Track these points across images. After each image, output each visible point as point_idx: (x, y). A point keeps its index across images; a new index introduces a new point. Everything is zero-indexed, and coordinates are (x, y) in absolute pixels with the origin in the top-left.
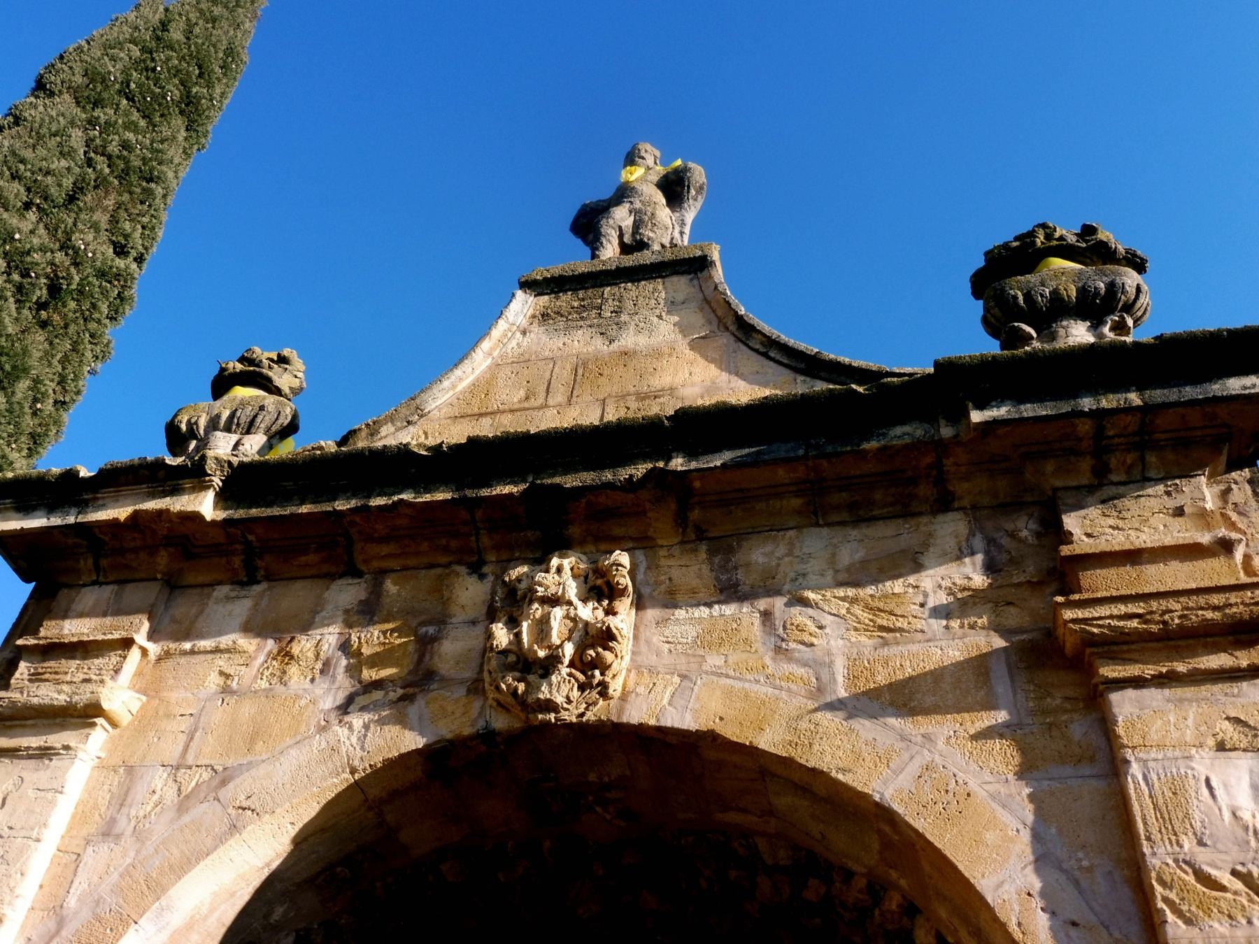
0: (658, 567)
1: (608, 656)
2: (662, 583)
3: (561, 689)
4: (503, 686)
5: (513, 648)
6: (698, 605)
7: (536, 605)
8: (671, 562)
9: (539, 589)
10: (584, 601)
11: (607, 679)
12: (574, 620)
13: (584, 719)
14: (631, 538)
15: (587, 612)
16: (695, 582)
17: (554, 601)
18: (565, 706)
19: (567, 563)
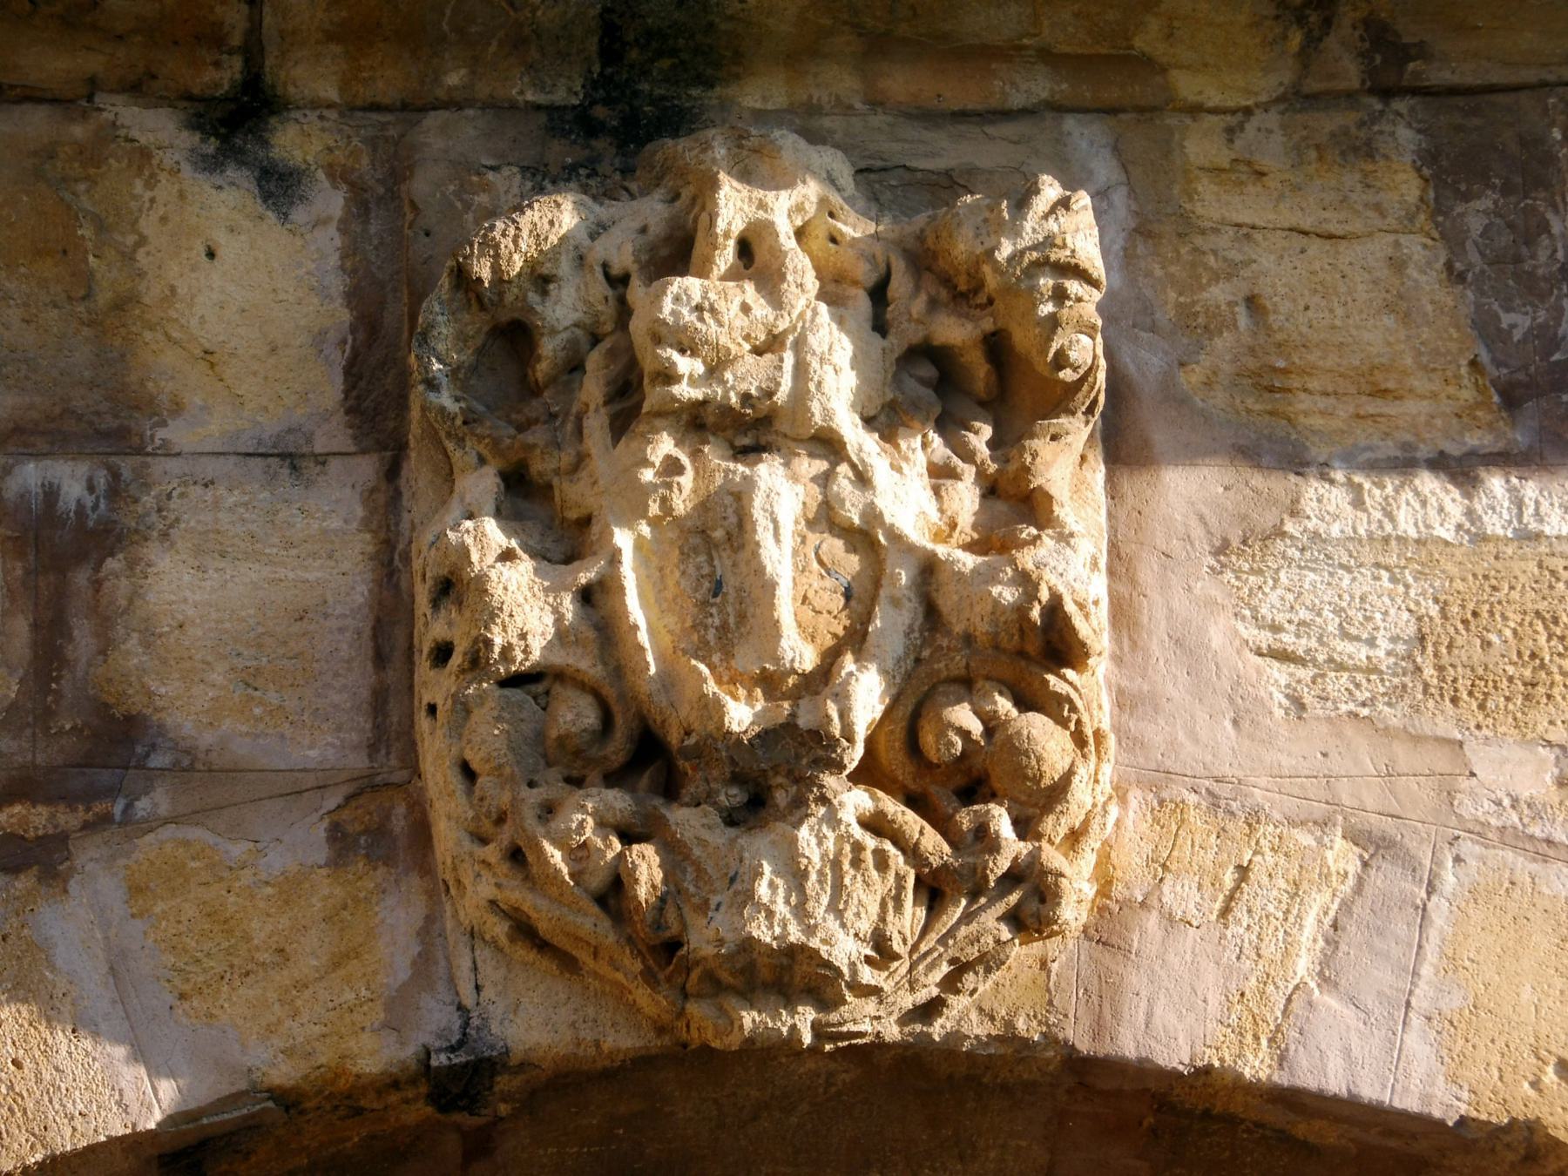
0: (1187, 226)
1: (1047, 741)
2: (1214, 324)
3: (836, 897)
4: (556, 856)
5: (585, 663)
6: (1404, 464)
7: (665, 446)
8: (1248, 207)
9: (687, 365)
10: (885, 419)
11: (1053, 857)
12: (865, 538)
13: (938, 1029)
14: (1047, 56)
15: (915, 494)
16: (1377, 336)
17: (752, 429)
18: (867, 975)
19: (786, 208)
